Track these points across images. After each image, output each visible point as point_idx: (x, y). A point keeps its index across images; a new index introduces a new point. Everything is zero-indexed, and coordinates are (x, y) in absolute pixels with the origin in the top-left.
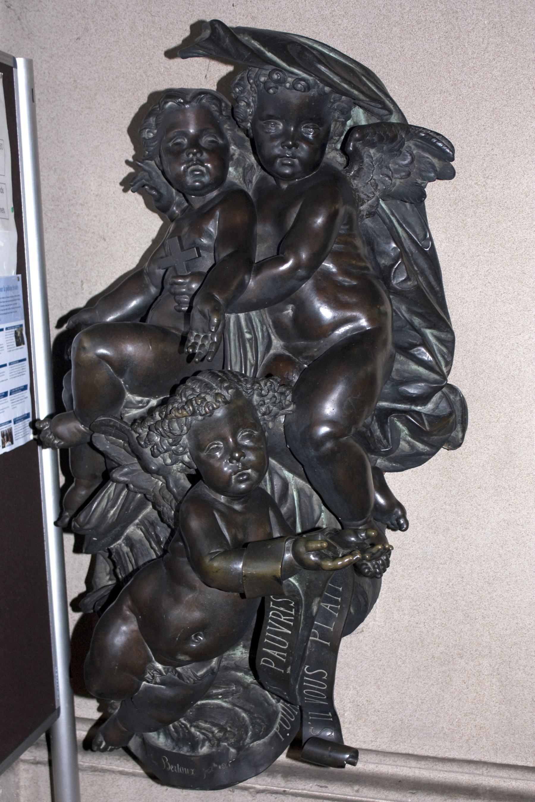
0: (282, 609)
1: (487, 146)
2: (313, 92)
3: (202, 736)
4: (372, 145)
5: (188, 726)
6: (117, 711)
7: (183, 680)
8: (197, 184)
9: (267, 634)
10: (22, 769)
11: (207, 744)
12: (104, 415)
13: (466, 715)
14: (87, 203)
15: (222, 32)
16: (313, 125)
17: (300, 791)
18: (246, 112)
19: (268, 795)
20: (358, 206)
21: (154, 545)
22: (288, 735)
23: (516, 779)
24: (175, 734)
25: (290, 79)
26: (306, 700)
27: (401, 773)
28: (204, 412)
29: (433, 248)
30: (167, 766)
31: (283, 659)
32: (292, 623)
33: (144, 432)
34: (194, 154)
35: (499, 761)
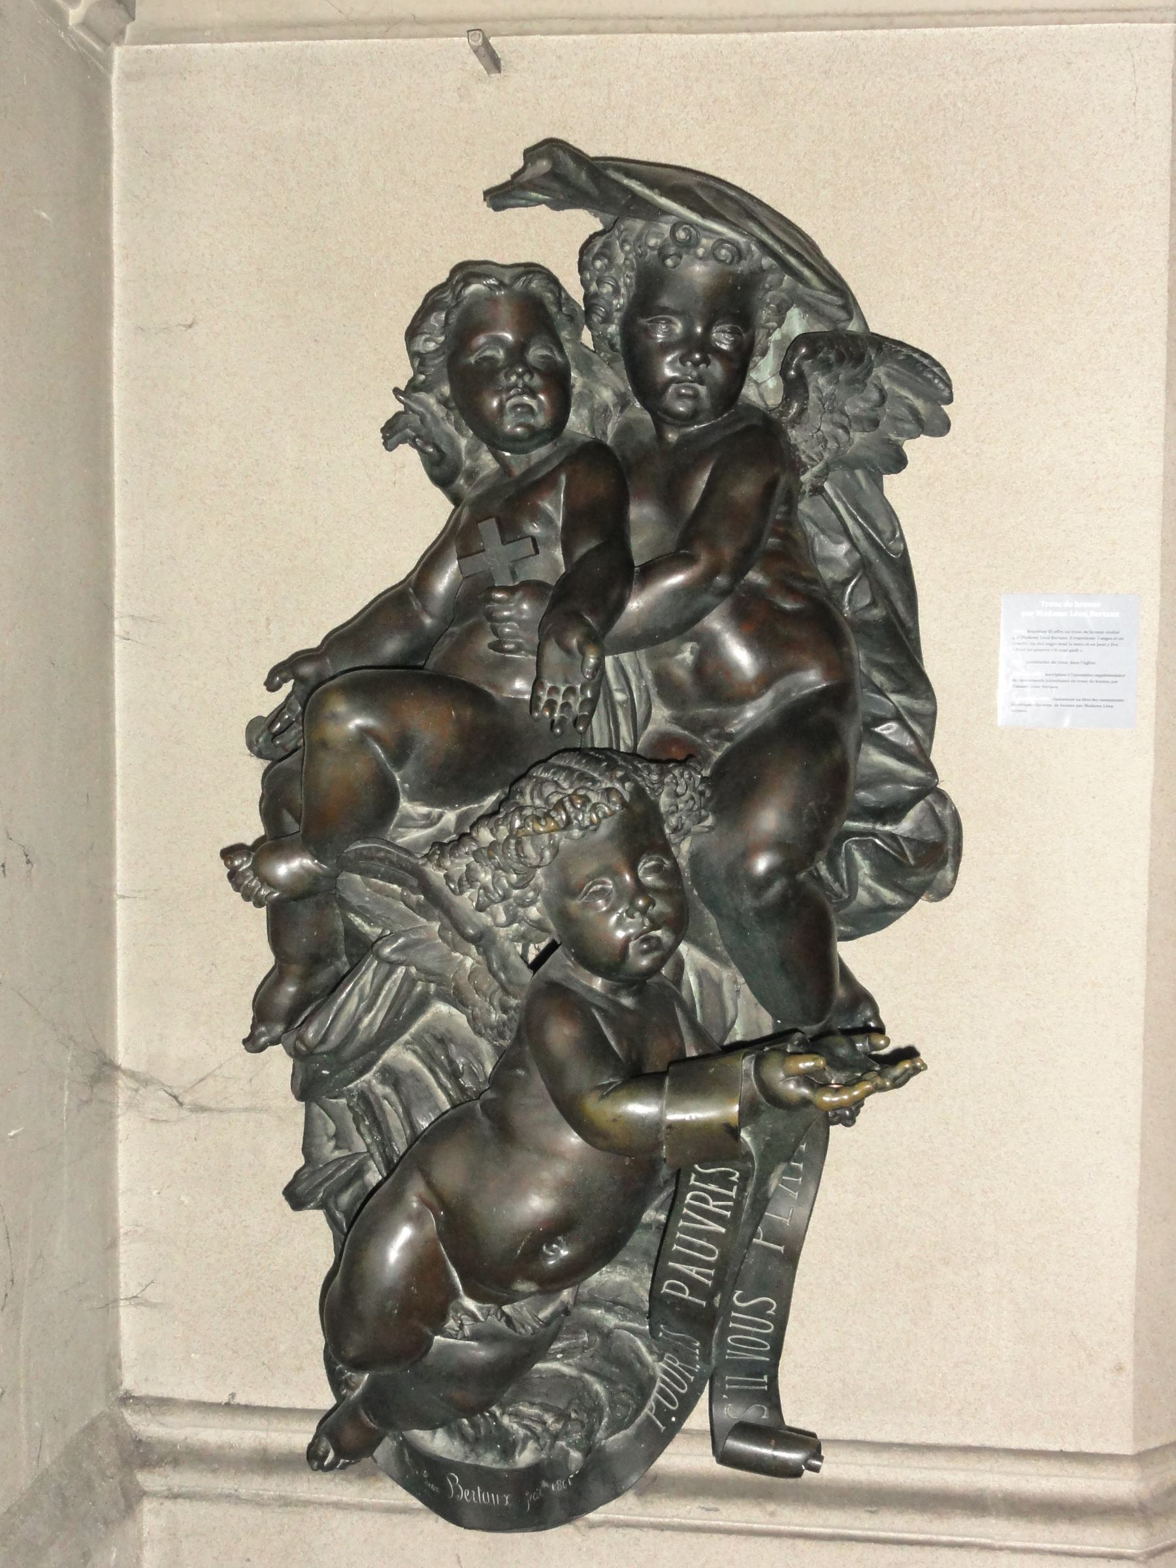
0: (712, 1187)
1: (981, 388)
2: (742, 267)
3: (522, 1432)
4: (826, 367)
5: (498, 1413)
6: (357, 1392)
7: (515, 1329)
8: (519, 429)
9: (678, 1235)
10: (145, 1510)
11: (531, 1445)
12: (364, 839)
13: (956, 1366)
14: (278, 481)
15: (571, 165)
16: (731, 328)
17: (667, 1520)
18: (611, 304)
19: (612, 1531)
20: (798, 476)
21: (444, 1080)
22: (673, 1419)
23: (1047, 1476)
24: (470, 1431)
25: (704, 241)
26: (729, 1355)
27: (845, 1477)
28: (587, 823)
29: (905, 553)
30: (457, 1492)
31: (706, 1281)
32: (729, 1214)
33: (459, 865)
34: (520, 376)
35: (1014, 1444)
